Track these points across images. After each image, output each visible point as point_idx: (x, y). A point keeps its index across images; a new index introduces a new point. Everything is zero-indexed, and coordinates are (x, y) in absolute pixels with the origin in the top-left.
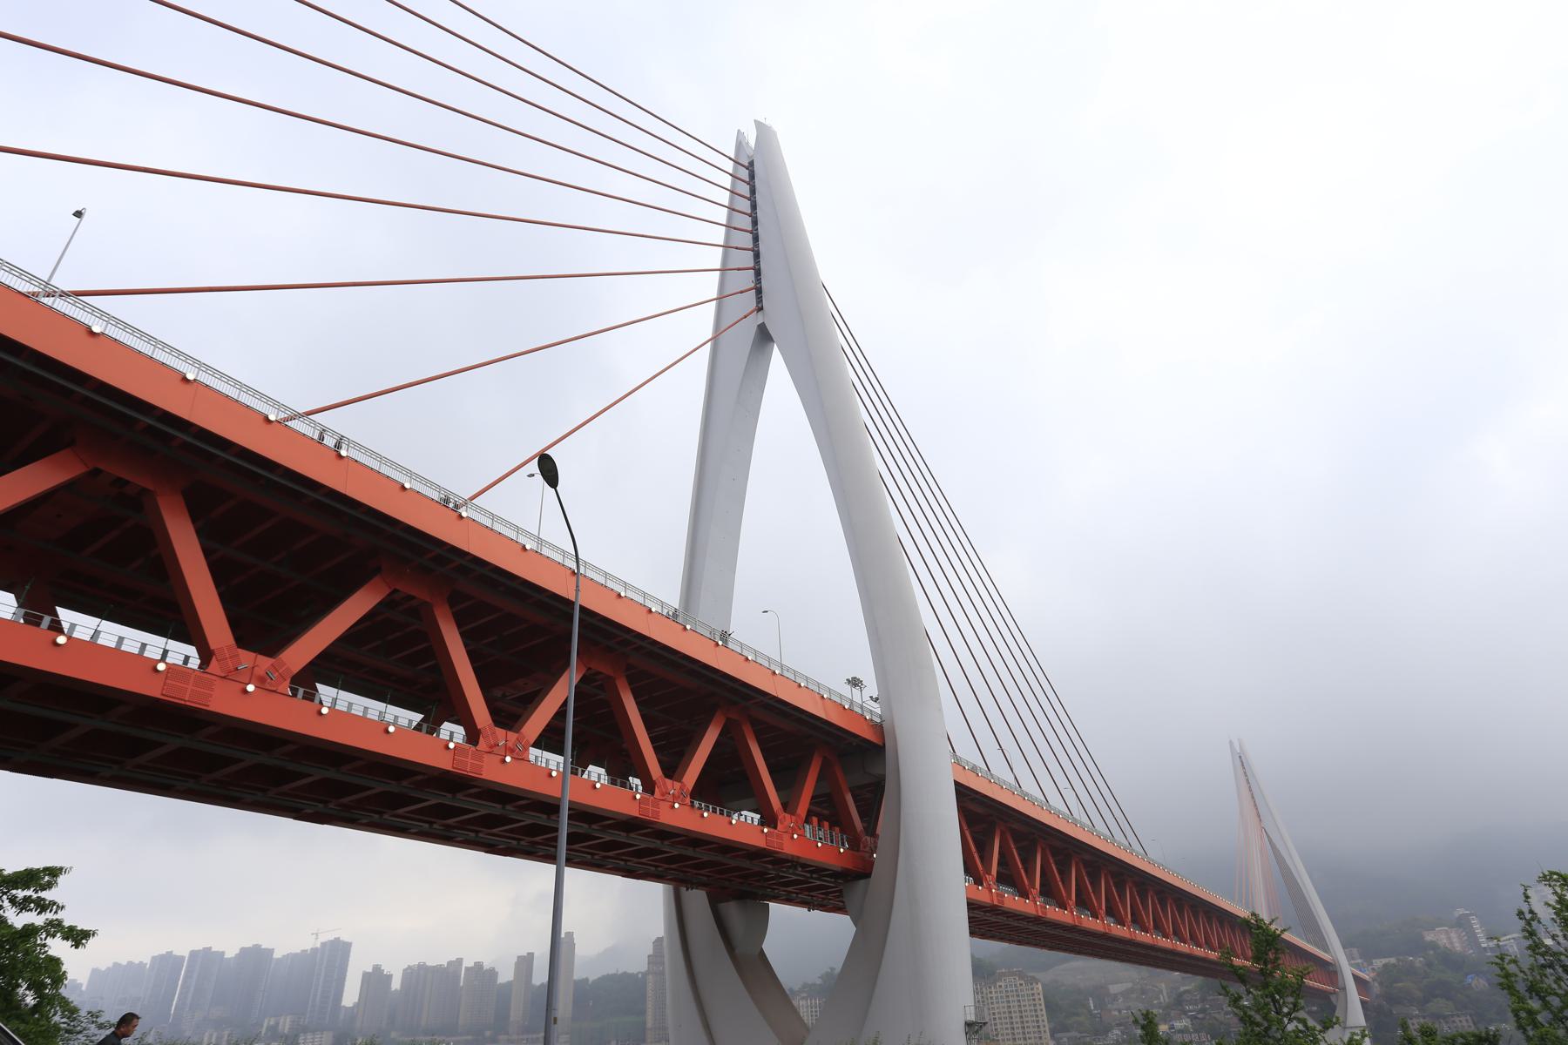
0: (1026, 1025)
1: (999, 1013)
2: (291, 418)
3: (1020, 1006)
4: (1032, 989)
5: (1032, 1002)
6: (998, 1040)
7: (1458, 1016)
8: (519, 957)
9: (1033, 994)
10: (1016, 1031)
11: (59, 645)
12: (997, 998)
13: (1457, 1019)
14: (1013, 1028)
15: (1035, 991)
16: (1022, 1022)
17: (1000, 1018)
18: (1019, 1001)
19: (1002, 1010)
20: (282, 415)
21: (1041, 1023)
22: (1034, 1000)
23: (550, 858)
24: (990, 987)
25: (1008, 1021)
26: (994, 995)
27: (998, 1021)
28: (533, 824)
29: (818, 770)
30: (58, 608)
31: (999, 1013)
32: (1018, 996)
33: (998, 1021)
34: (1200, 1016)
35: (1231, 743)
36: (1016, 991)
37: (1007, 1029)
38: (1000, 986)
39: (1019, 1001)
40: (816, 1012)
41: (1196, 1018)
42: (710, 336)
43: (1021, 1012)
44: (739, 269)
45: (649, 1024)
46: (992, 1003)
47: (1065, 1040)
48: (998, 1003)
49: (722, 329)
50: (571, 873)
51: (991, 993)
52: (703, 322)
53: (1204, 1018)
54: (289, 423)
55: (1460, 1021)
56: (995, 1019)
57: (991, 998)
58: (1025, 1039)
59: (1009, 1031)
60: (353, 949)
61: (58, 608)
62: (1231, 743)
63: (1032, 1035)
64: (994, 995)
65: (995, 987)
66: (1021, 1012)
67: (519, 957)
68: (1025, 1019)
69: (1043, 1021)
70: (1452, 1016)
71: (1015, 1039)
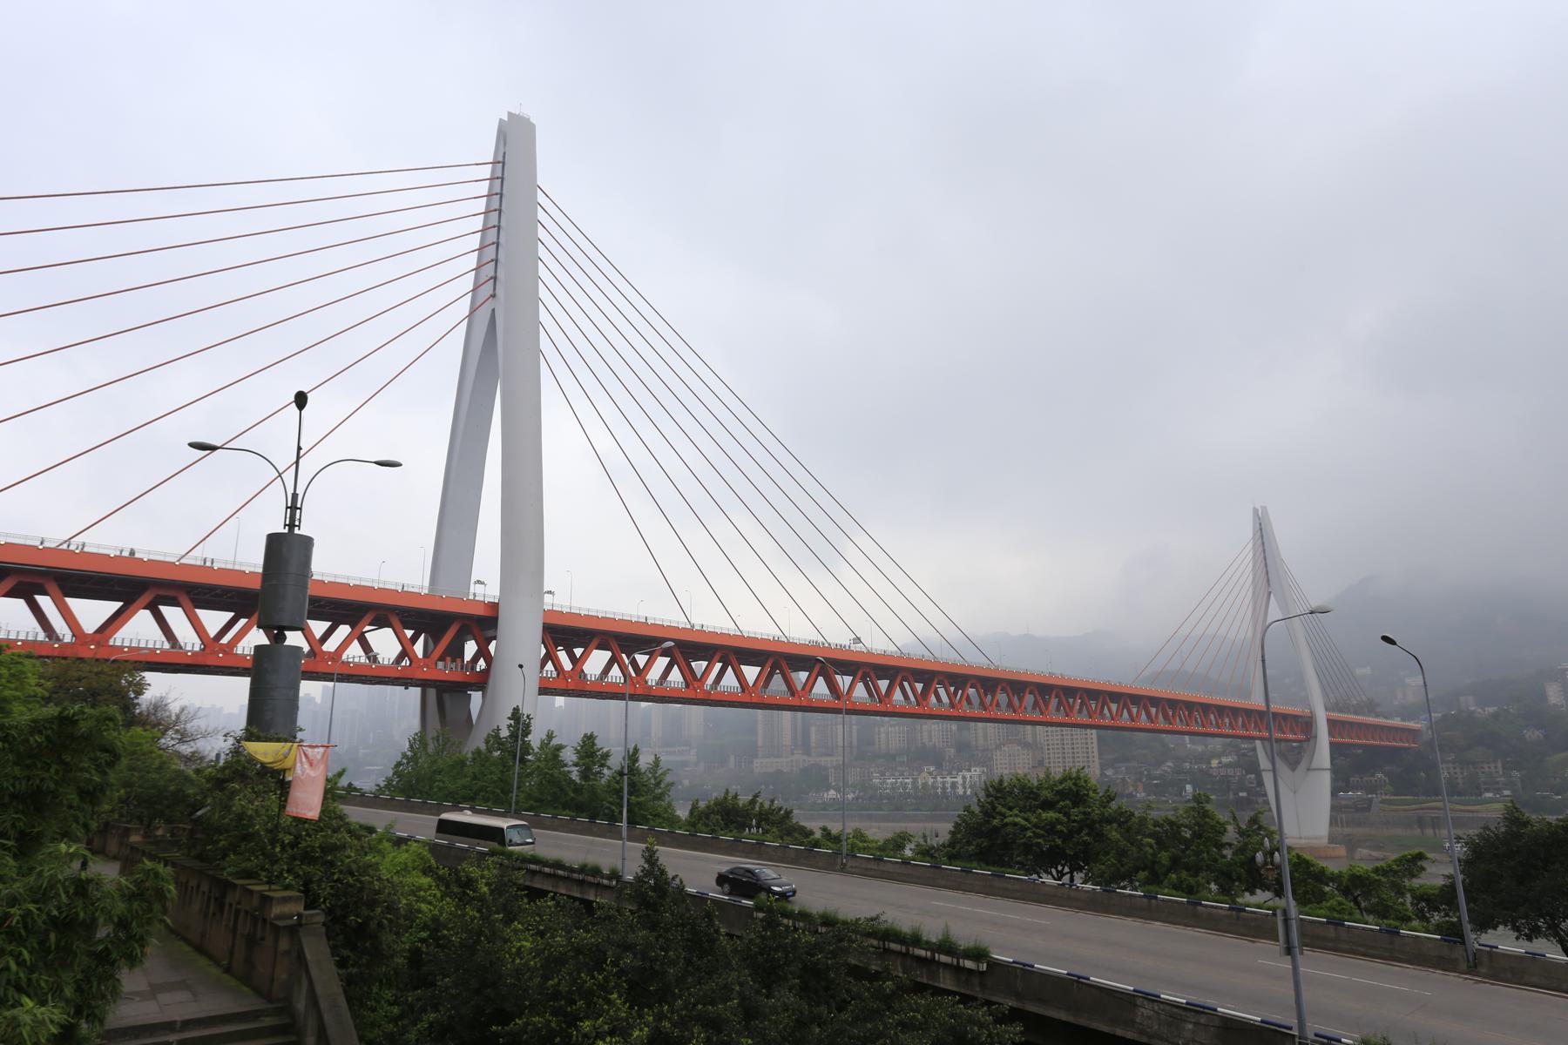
1: (1053, 744)
3: (1072, 739)
7: (1488, 763)
10: (1067, 760)
13: (1486, 766)
14: (1065, 758)
23: (624, 700)
29: (456, 631)
30: (330, 623)
31: (1054, 762)
33: (1051, 751)
37: (1059, 758)
45: (760, 743)
47: (1123, 769)
48: (1052, 736)
49: (484, 262)
50: (629, 702)
52: (468, 282)
55: (1489, 767)
59: (1060, 760)
61: (330, 623)
63: (1080, 755)
68: (1076, 760)
69: (1093, 752)
70: (1482, 762)
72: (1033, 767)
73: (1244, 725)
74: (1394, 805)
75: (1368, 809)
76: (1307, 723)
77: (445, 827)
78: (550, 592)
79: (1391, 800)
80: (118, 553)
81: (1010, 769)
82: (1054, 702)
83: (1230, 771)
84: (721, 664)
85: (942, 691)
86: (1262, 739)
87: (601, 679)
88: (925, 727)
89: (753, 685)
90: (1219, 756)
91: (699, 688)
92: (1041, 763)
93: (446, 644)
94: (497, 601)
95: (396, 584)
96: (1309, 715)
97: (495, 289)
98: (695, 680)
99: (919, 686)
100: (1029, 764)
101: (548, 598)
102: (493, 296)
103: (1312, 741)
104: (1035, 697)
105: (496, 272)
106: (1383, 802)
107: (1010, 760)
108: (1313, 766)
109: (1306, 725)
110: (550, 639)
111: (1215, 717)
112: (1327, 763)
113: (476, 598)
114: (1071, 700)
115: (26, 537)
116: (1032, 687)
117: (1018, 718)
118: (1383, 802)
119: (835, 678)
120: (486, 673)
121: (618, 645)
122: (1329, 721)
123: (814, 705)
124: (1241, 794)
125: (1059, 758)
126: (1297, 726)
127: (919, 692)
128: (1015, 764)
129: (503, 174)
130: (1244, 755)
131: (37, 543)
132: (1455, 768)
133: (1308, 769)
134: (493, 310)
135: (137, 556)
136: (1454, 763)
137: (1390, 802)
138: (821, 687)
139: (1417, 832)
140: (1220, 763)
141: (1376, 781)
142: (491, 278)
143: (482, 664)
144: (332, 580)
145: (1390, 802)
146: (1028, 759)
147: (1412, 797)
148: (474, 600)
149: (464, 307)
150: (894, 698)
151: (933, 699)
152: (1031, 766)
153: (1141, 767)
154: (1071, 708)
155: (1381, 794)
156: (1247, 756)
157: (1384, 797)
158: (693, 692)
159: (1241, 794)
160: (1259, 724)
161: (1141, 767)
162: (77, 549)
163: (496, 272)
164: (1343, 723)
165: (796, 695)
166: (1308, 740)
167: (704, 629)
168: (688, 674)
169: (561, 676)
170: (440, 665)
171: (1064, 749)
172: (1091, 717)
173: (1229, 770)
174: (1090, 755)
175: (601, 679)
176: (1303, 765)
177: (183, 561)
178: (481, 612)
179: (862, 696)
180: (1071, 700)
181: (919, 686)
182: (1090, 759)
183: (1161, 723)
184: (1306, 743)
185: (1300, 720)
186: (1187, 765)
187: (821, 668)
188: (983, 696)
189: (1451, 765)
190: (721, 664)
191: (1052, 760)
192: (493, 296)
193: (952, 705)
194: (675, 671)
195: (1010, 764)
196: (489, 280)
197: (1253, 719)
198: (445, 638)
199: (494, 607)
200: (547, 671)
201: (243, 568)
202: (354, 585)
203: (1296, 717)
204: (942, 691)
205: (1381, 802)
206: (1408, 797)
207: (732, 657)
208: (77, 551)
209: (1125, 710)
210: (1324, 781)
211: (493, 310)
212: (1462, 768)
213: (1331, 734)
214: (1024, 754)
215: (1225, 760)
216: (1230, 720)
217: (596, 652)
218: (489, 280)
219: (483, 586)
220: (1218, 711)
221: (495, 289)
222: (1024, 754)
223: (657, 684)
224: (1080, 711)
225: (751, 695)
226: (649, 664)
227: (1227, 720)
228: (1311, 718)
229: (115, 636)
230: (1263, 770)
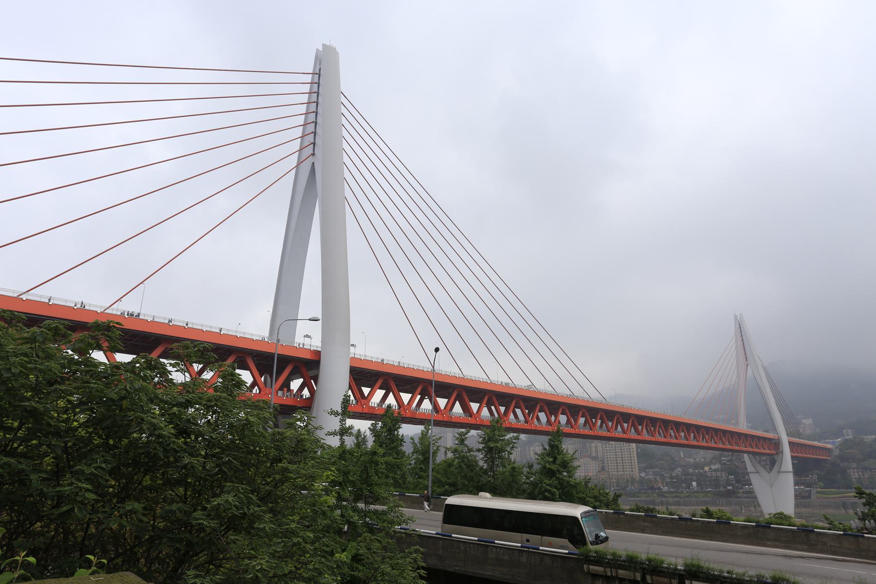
0: (623, 456)
2: (106, 310)
9: (630, 449)
11: (346, 532)
12: (609, 450)
15: (631, 447)
17: (611, 461)
18: (622, 452)
19: (612, 456)
20: (103, 310)
21: (632, 458)
22: (630, 452)
24: (606, 445)
25: (614, 454)
26: (608, 449)
31: (611, 466)
33: (609, 462)
34: (728, 463)
37: (614, 466)
38: (612, 444)
39: (622, 452)
40: (518, 454)
42: (296, 165)
43: (622, 457)
44: (301, 104)
46: (607, 453)
47: (651, 473)
51: (606, 447)
54: (106, 311)
56: (608, 461)
58: (624, 471)
64: (608, 449)
65: (609, 445)
66: (622, 457)
69: (634, 457)
71: (618, 471)
72: (599, 472)
73: (695, 437)
74: (825, 494)
75: (809, 497)
76: (775, 443)
77: (454, 515)
78: (353, 345)
79: (821, 491)
80: (152, 319)
81: (585, 473)
82: (582, 420)
83: (719, 474)
84: (420, 396)
85: (518, 411)
86: (748, 453)
87: (416, 411)
88: (593, 445)
89: (477, 413)
90: (709, 464)
91: (365, 404)
92: (603, 469)
93: (285, 378)
94: (319, 349)
95: (165, 319)
96: (778, 439)
97: (314, 150)
98: (362, 399)
99: (502, 409)
100: (596, 470)
101: (352, 349)
102: (313, 154)
103: (780, 455)
104: (567, 417)
105: (315, 140)
106: (818, 492)
107: (585, 467)
108: (781, 471)
109: (776, 444)
110: (394, 385)
111: (674, 432)
112: (790, 468)
113: (305, 347)
114: (594, 420)
115: (66, 301)
116: (602, 413)
117: (574, 432)
118: (818, 492)
119: (499, 408)
120: (311, 399)
121: (395, 384)
122: (790, 443)
123: (513, 427)
124: (728, 488)
125: (614, 466)
126: (771, 446)
127: (503, 412)
128: (588, 470)
129: (318, 90)
130: (725, 464)
131: (73, 305)
132: (858, 472)
133: (779, 472)
134: (313, 163)
135: (141, 317)
136: (857, 469)
137: (823, 493)
138: (458, 409)
139: (843, 511)
140: (710, 469)
141: (809, 480)
142: (312, 143)
143: (306, 393)
144: (209, 329)
145: (823, 493)
146: (596, 467)
147: (835, 490)
148: (303, 348)
149: (293, 160)
150: (482, 414)
151: (512, 416)
152: (597, 471)
153: (662, 471)
154: (594, 424)
155: (816, 488)
156: (725, 464)
157: (818, 490)
158: (442, 416)
159: (728, 488)
160: (745, 442)
161: (662, 471)
162: (75, 306)
163: (315, 140)
164: (798, 444)
165: (440, 413)
166: (777, 454)
167: (401, 365)
168: (466, 409)
169: (359, 403)
170: (280, 393)
171: (617, 460)
172: (609, 431)
173: (718, 473)
174: (633, 464)
175: (416, 411)
176: (776, 468)
177: (108, 311)
178: (308, 356)
179: (485, 415)
180: (594, 420)
181: (502, 409)
182: (633, 467)
183: (633, 434)
184: (776, 455)
185: (773, 441)
186: (691, 470)
187: (488, 399)
188: (527, 416)
189: (855, 470)
190: (420, 396)
191: (610, 467)
192: (313, 154)
193: (526, 421)
194: (406, 401)
195: (585, 470)
196: (311, 144)
197: (761, 443)
198: (453, 396)
199: (318, 353)
200: (422, 409)
201: (146, 318)
202: (256, 340)
203: (770, 439)
204: (518, 411)
205: (817, 493)
206: (833, 490)
207: (393, 385)
208: (75, 308)
209: (619, 426)
210: (790, 478)
211: (313, 163)
212: (863, 472)
213: (792, 451)
214: (593, 464)
215: (713, 467)
216: (685, 434)
217: (378, 391)
218: (311, 144)
219: (309, 339)
220: (745, 437)
221: (314, 150)
222: (593, 464)
223: (378, 405)
224: (601, 427)
225: (363, 407)
226: (371, 394)
227: (682, 434)
228: (779, 440)
229: (371, 401)
230: (750, 473)
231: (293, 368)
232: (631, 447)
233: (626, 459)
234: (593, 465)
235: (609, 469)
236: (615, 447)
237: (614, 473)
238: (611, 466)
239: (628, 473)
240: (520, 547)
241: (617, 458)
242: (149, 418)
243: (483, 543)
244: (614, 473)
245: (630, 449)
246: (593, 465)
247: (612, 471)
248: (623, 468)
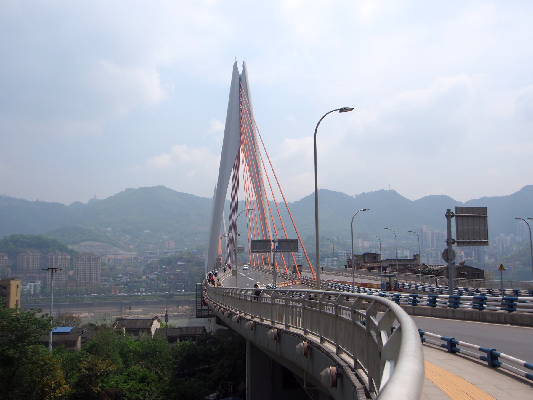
4: (97, 261)
5: (96, 266)
6: (78, 280)
8: (38, 200)
9: (97, 263)
12: (81, 263)
16: (90, 274)
18: (90, 265)
19: (82, 273)
27: (79, 275)
28: (444, 260)
32: (90, 263)
33: (79, 275)
35: (235, 65)
36: (90, 261)
37: (83, 276)
41: (158, 275)
53: (160, 275)
57: (78, 263)
58: (90, 280)
60: (486, 246)
62: (235, 65)
63: (93, 279)
67: (38, 200)
68: (95, 273)
231: (340, 354)
232: (98, 262)
233: (94, 270)
234: (64, 275)
235: (77, 278)
236: (86, 261)
237: (82, 281)
238: (80, 278)
239: (93, 281)
240: (426, 306)
241: (86, 265)
242: (353, 300)
243: (469, 279)
244: (82, 281)
245: (97, 263)
246: (64, 275)
247: (80, 280)
248: (90, 278)
